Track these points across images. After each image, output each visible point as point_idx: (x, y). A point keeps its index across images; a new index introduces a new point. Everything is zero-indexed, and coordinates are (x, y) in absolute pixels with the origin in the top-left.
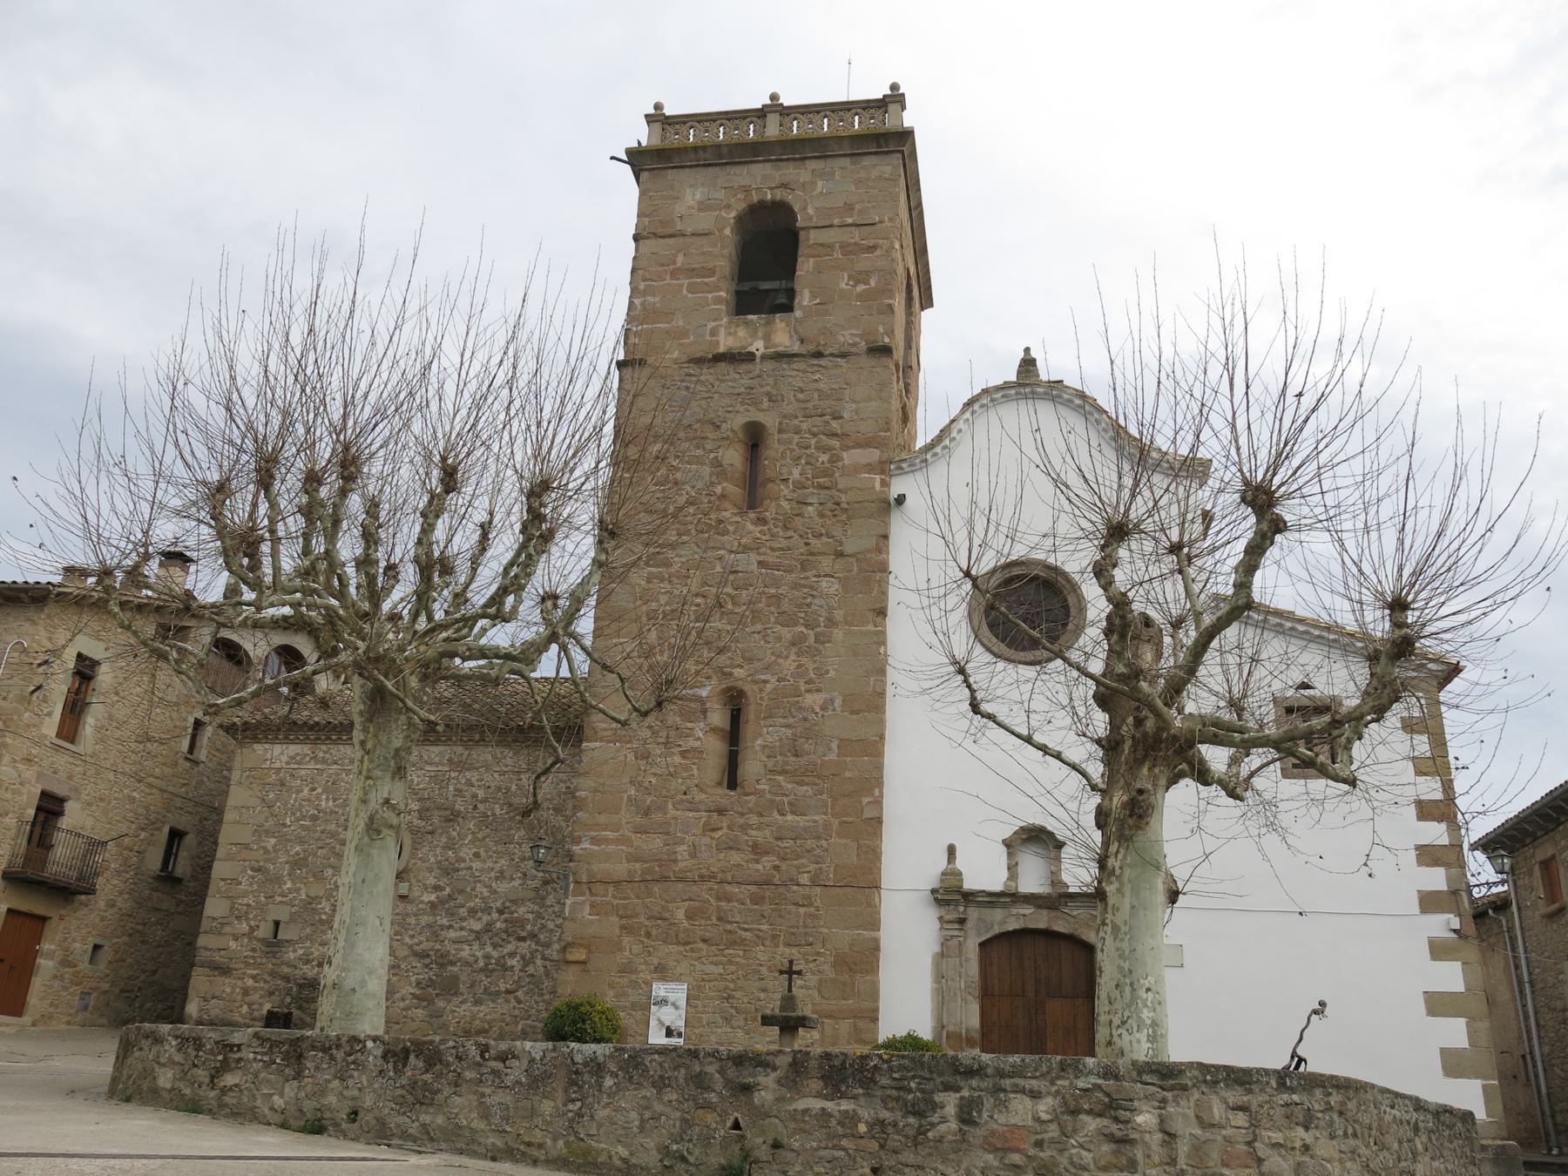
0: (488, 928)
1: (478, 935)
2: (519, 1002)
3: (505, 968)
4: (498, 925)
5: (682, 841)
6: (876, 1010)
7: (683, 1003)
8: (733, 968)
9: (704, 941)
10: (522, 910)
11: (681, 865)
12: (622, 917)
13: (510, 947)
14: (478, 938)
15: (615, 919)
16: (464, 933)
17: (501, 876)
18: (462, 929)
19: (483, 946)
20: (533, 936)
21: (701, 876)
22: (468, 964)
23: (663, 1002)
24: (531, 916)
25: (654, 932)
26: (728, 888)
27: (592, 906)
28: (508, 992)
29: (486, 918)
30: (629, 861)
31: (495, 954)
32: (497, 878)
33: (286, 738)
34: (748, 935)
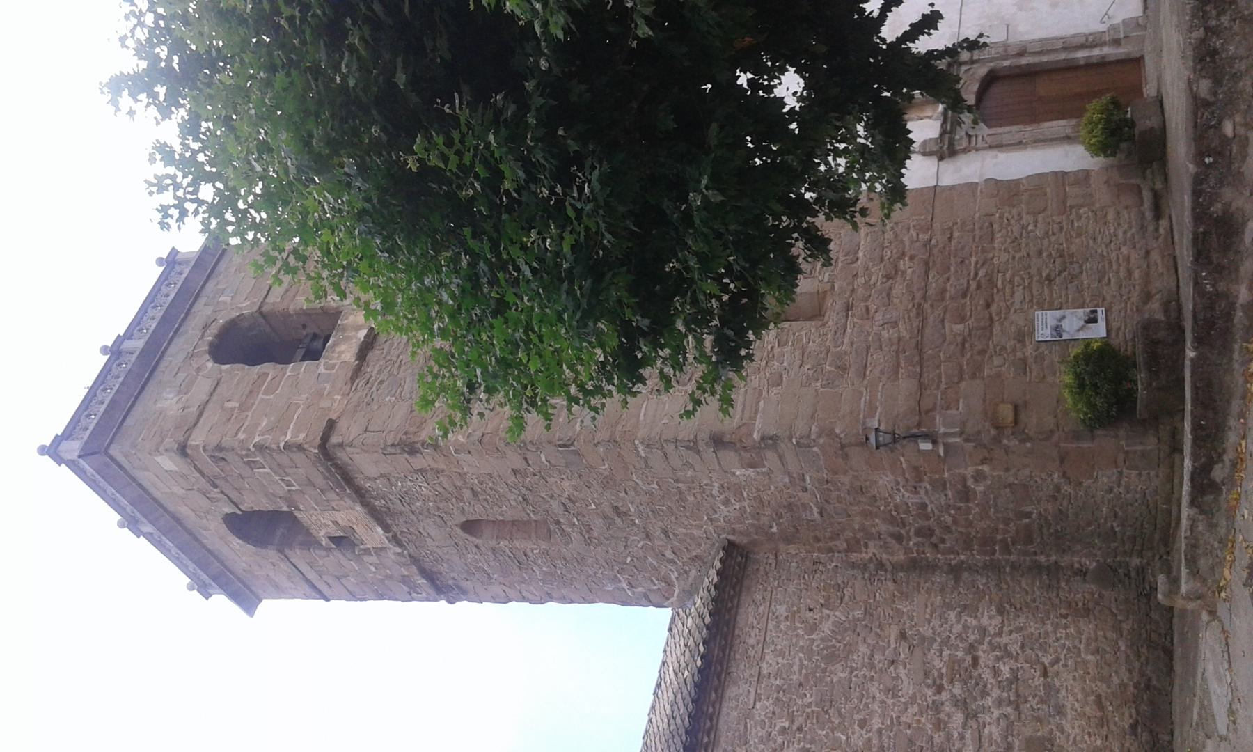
0: (961, 704)
1: (970, 715)
2: (1057, 661)
3: (1015, 679)
4: (957, 691)
5: (879, 335)
6: (1056, 173)
7: (1058, 313)
8: (1017, 279)
9: (988, 306)
10: (938, 663)
11: (904, 333)
12: (961, 379)
13: (987, 675)
14: (975, 716)
15: (963, 385)
16: (968, 735)
17: (892, 691)
18: (962, 738)
19: (985, 710)
20: (971, 648)
21: (918, 315)
22: (1010, 726)
23: (1058, 330)
24: (946, 653)
25: (979, 347)
26: (930, 292)
27: (948, 408)
28: (1045, 674)
29: (947, 708)
30: (897, 379)
31: (996, 693)
32: (895, 696)
33: (729, 610)
34: (981, 273)
